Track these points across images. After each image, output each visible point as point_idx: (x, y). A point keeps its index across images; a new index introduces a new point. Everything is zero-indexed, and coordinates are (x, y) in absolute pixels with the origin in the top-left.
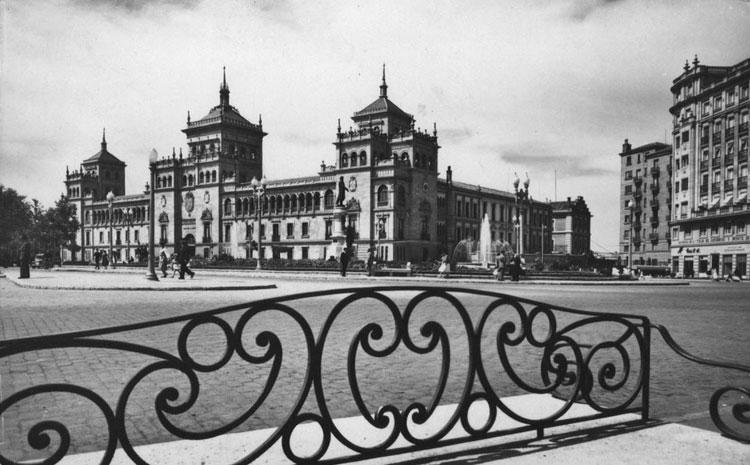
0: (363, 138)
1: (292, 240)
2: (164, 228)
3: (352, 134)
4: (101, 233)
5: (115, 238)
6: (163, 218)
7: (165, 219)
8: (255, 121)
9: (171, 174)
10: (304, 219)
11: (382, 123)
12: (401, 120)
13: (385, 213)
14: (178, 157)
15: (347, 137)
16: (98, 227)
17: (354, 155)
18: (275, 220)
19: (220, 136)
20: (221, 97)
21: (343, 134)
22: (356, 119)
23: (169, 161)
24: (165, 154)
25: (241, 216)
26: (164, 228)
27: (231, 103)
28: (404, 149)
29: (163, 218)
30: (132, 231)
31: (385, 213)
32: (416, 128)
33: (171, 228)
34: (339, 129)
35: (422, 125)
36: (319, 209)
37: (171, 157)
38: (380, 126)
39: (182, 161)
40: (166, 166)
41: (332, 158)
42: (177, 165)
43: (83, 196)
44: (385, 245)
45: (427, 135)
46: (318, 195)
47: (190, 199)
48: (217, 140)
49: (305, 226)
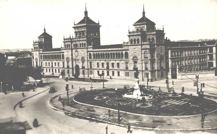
0: (138, 34)
1: (113, 69)
2: (68, 62)
3: (133, 32)
4: (46, 63)
5: (51, 65)
6: (68, 58)
7: (37, 60)
8: (97, 22)
9: (69, 43)
10: (58, 61)
11: (144, 27)
12: (151, 25)
13: (147, 61)
14: (72, 37)
15: (135, 33)
16: (45, 61)
17: (135, 40)
18: (107, 61)
19: (86, 30)
20: (85, 14)
21: (131, 32)
22: (39, 38)
23: (69, 39)
24: (67, 37)
25: (44, 60)
26: (68, 62)
27: (88, 16)
28: (151, 36)
29: (68, 58)
30: (54, 62)
31: (147, 61)
32: (156, 29)
33: (70, 62)
34: (64, 38)
35: (158, 27)
36: (123, 58)
37: (37, 41)
38: (143, 28)
39: (73, 39)
40: (68, 41)
41: (127, 40)
42: (71, 40)
43: (87, 47)
44: (92, 70)
45: (160, 30)
46: (122, 53)
47: (77, 52)
48: (85, 31)
49: (118, 64)
